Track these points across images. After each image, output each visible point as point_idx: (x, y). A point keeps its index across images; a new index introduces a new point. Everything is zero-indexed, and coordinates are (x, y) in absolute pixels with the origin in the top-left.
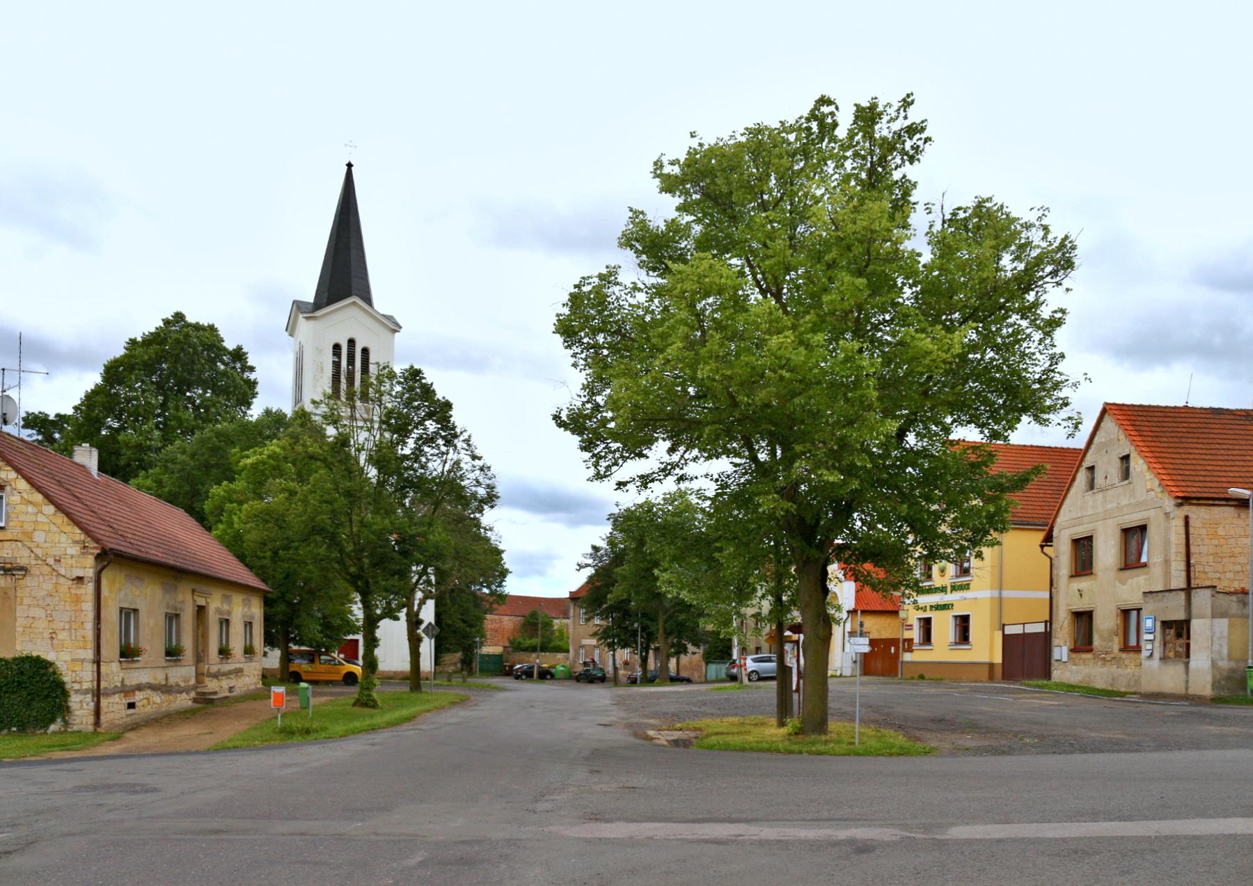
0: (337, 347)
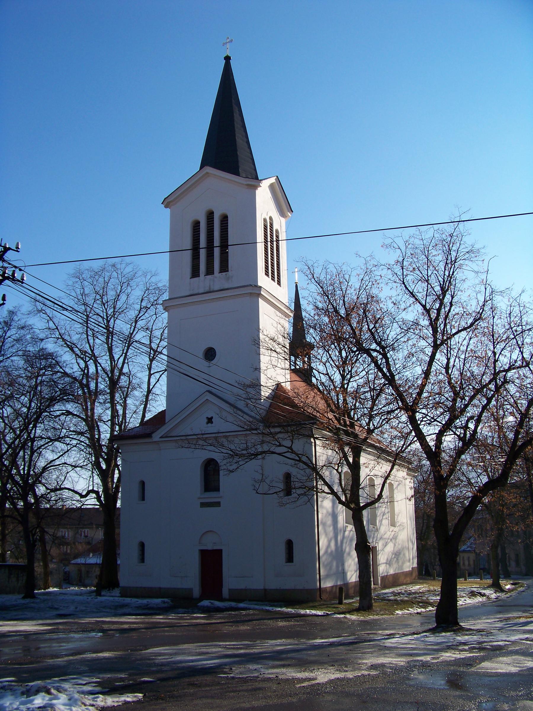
0: (196, 225)
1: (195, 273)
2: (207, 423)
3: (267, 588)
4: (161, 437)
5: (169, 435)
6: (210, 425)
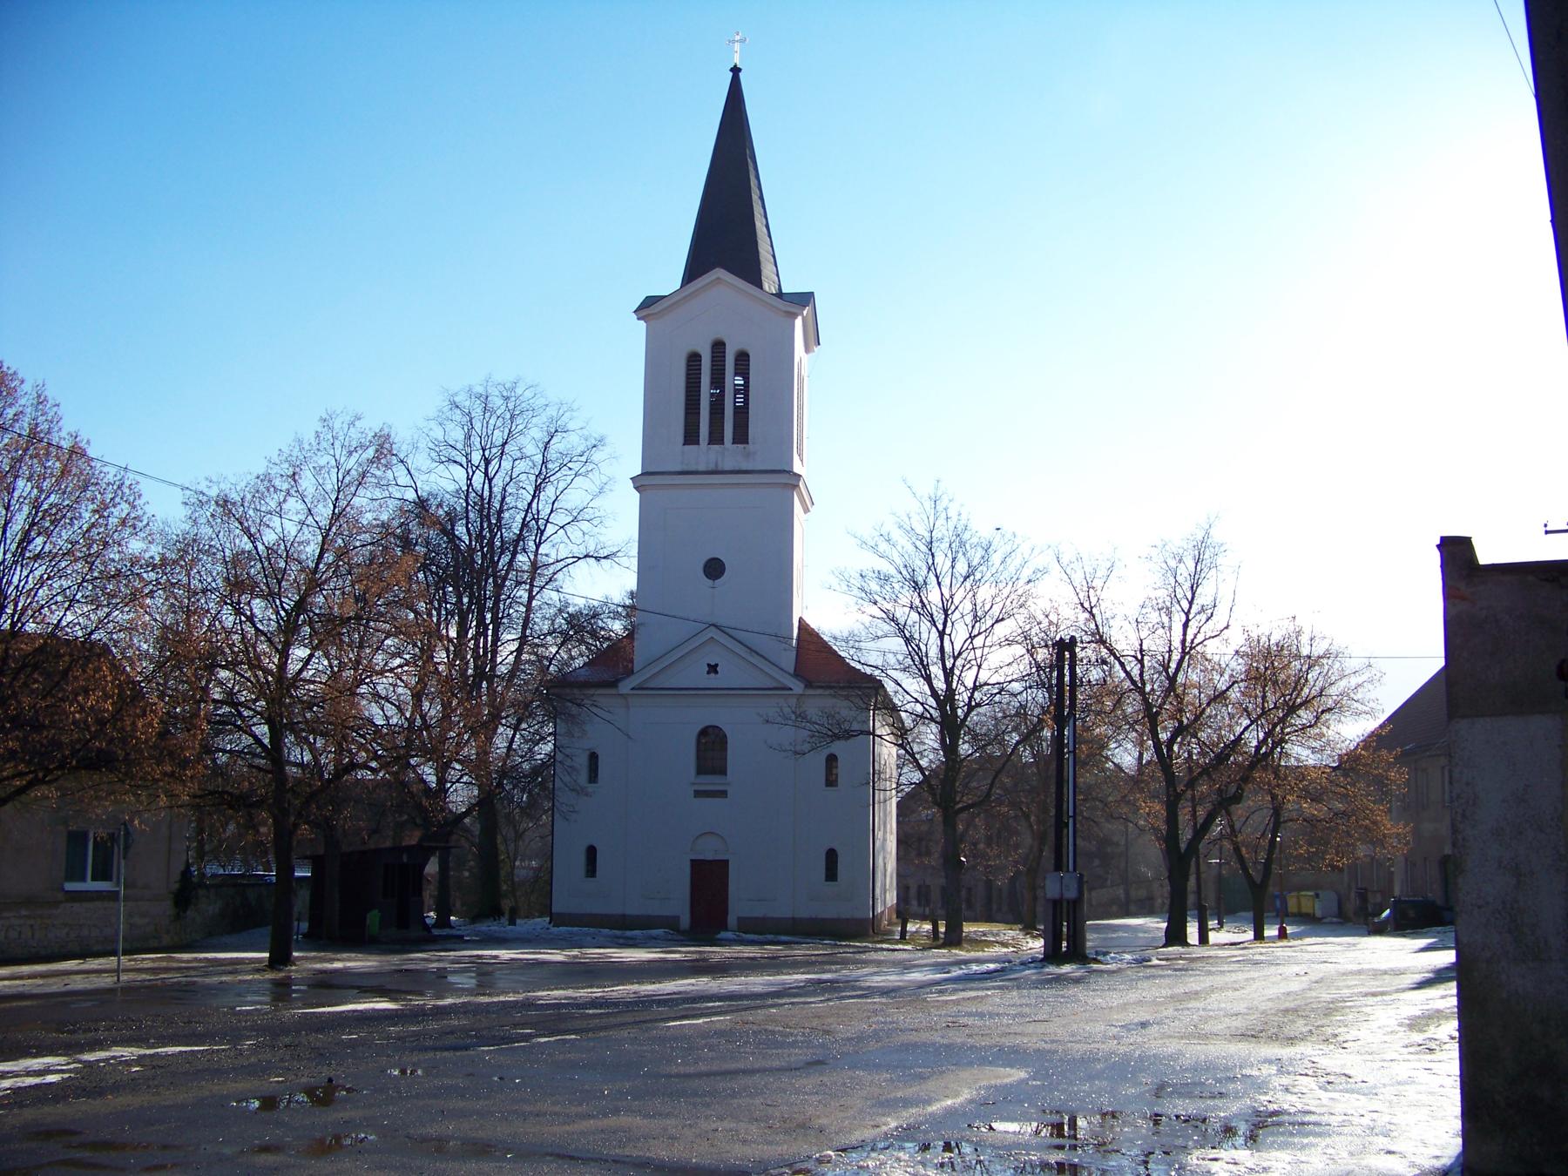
0: (694, 359)
1: (691, 437)
2: (708, 673)
3: (796, 916)
4: (633, 689)
5: (645, 686)
6: (712, 675)
